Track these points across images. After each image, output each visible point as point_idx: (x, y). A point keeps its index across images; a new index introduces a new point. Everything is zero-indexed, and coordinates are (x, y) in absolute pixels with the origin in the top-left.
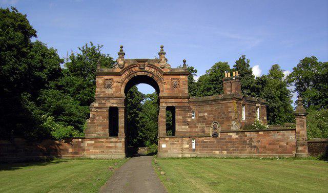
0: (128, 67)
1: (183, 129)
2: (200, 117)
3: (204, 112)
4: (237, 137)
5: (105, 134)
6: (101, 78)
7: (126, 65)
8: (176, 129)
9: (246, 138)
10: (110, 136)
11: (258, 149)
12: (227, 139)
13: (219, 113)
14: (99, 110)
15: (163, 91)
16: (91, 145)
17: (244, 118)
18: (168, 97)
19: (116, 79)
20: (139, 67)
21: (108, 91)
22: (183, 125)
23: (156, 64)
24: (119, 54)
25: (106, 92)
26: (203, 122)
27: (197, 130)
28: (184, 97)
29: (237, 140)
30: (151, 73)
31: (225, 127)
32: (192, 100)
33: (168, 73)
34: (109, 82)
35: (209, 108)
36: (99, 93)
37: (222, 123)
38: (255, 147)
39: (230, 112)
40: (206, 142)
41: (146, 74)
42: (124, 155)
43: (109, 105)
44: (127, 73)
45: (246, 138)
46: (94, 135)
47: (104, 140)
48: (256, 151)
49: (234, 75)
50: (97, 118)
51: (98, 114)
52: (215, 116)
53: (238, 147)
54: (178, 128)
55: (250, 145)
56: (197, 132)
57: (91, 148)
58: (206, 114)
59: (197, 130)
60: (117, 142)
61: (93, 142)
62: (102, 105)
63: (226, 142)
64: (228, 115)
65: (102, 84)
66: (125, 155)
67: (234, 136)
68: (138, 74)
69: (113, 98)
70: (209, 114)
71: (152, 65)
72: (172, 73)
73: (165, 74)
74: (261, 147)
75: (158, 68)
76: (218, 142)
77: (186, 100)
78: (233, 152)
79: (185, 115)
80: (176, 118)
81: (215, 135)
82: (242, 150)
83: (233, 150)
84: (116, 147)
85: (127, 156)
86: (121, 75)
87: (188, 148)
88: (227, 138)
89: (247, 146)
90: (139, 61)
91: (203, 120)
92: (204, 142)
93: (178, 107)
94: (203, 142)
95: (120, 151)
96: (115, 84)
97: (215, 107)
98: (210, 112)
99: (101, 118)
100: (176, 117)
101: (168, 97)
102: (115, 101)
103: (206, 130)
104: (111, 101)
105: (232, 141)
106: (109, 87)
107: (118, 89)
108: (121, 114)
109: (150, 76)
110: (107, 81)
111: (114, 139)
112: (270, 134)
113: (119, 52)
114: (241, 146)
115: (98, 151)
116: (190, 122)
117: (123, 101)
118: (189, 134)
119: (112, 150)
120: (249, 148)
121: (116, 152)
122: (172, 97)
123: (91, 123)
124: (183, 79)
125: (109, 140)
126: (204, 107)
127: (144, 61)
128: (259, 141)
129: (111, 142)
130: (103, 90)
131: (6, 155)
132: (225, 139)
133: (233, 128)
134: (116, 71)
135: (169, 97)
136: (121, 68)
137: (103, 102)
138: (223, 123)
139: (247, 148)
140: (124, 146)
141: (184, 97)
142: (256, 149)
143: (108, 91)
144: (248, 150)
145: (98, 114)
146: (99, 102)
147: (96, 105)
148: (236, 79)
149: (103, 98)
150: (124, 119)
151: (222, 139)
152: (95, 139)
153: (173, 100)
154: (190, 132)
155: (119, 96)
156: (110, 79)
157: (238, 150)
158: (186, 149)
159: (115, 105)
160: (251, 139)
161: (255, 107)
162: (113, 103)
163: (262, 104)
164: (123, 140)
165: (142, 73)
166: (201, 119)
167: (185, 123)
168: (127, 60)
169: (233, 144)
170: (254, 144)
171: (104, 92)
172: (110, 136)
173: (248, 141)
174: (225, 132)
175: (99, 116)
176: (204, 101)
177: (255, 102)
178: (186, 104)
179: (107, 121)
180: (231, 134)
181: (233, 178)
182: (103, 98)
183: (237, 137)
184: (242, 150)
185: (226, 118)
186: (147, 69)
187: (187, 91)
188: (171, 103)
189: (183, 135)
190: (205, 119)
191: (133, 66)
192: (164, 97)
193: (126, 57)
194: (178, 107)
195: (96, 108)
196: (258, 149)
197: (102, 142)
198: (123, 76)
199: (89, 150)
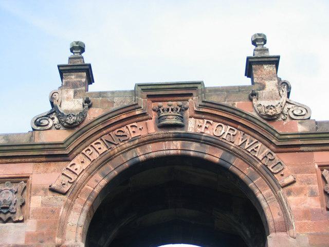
20: (160, 118)
24: (64, 71)
30: (214, 143)
41: (193, 149)
44: (99, 149)
73: (289, 145)
86: (66, 158)
96: (36, 202)
109: (216, 156)
156: (15, 180)
165: (174, 147)
186: (192, 126)
198: (79, 164)
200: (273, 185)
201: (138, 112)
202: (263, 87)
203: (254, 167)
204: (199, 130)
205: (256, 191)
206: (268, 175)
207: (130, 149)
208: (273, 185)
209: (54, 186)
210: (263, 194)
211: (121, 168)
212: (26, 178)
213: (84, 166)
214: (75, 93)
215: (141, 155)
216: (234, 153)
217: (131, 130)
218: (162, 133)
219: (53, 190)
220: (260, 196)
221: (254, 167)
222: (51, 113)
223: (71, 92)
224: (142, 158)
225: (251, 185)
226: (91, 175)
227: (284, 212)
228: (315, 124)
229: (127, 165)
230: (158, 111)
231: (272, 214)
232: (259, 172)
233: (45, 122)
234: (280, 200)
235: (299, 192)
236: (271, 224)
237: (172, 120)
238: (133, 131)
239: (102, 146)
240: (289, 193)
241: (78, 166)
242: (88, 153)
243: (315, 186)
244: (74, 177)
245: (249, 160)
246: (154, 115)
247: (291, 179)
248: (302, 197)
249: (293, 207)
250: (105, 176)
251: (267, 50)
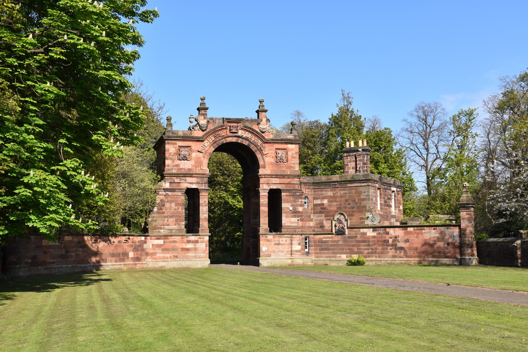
0: (214, 129)
1: (292, 223)
2: (315, 205)
3: (324, 198)
4: (374, 234)
5: (180, 230)
6: (172, 144)
7: (211, 127)
8: (283, 223)
9: (387, 237)
10: (188, 232)
11: (405, 252)
12: (359, 238)
13: (346, 200)
14: (170, 193)
15: (264, 167)
16: (159, 246)
17: (71, 152)
18: (271, 176)
19: (195, 146)
20: (230, 130)
21: (184, 164)
22: (292, 217)
23: (255, 127)
24: (198, 109)
25: (181, 167)
26: (321, 212)
27: (312, 224)
28: (294, 176)
29: (373, 239)
30: (246, 139)
31: (354, 220)
32: (305, 181)
33: (272, 140)
34: (184, 152)
35: (330, 193)
36: (170, 168)
37: (351, 215)
38: (402, 248)
39: (364, 200)
40: (325, 242)
41: (240, 141)
42: (209, 261)
43: (185, 185)
44: (212, 138)
45: (387, 237)
46: (162, 231)
47: (177, 238)
48: (402, 254)
49: (360, 144)
50: (167, 205)
51: (170, 199)
52: (340, 205)
53: (376, 249)
54: (287, 221)
55: (394, 246)
56: (311, 227)
57: (159, 251)
58: (325, 202)
59: (312, 224)
60: (197, 242)
61: (161, 242)
62: (174, 186)
63: (358, 241)
64: (360, 203)
65: (174, 154)
66: (210, 262)
67: (370, 233)
68: (229, 140)
69: (191, 175)
70: (331, 202)
71: (249, 128)
72: (277, 140)
73: (267, 142)
74: (410, 248)
75: (257, 132)
76: (345, 241)
77: (296, 181)
78: (369, 257)
79: (295, 201)
80: (283, 206)
81: (340, 232)
82: (382, 253)
83: (368, 253)
84: (196, 249)
85: (212, 263)
86: (202, 141)
87: (300, 251)
88: (359, 236)
89: (389, 248)
90: (230, 121)
91: (321, 209)
92: (323, 242)
93: (286, 191)
94: (321, 241)
95: (202, 255)
96: (194, 155)
97: (340, 192)
98: (332, 199)
99: (173, 205)
100: (283, 204)
101: (271, 176)
102: (194, 180)
103: (327, 224)
104: (189, 179)
105: (366, 240)
106: (185, 158)
107: (199, 163)
108: (204, 200)
109: (246, 143)
110: (182, 149)
111: (192, 238)
112: (423, 231)
113: (207, 111)
114: (380, 248)
115: (168, 255)
116: (302, 212)
117: (206, 180)
118: (300, 230)
119: (191, 254)
120: (393, 251)
121: (195, 257)
122: (277, 176)
123: (158, 213)
124: (292, 149)
125: (185, 239)
126: (323, 191)
127: (238, 121)
128: (407, 241)
129: (189, 242)
130: (177, 162)
131: (53, 263)
132: (356, 237)
133: (368, 222)
134: (196, 135)
135: (273, 175)
136: (203, 131)
137: (177, 180)
138: (352, 215)
139: (389, 250)
140: (208, 248)
141: (294, 176)
142: (402, 251)
143: (184, 164)
144: (392, 252)
145: (170, 199)
146: (170, 181)
147: (167, 185)
148: (363, 150)
149: (177, 175)
150: (207, 208)
151: (351, 237)
152: (166, 237)
153: (277, 180)
154: (302, 227)
155: (201, 172)
156: (188, 147)
157: (375, 253)
158: (297, 251)
159: (194, 186)
160: (396, 237)
161: (390, 192)
162: (191, 183)
163: (398, 187)
164: (207, 238)
165: (234, 140)
166: (318, 209)
167: (295, 213)
168: (212, 119)
169: (369, 245)
170: (400, 245)
171: (177, 165)
172: (188, 232)
173: (391, 241)
174: (356, 228)
175: (171, 202)
176: (322, 183)
177: (390, 185)
178: (297, 187)
179: (182, 211)
180: (365, 230)
181: (403, 300)
182: (177, 175)
183: (374, 234)
184: (383, 253)
185: (358, 207)
186: (240, 133)
187: (297, 168)
188: (275, 184)
189: (293, 232)
190: (325, 208)
191: (222, 128)
192: (266, 176)
193: (210, 114)
194: (286, 191)
195: (165, 190)
196: (405, 252)
197: (175, 242)
198: (206, 143)
199: (154, 254)
200: (263, 155)
201: (224, 127)
202: (262, 121)
203: (257, 148)
204: (242, 134)
205: (257, 155)
206: (261, 150)
207: (221, 139)
208: (263, 155)
209: (199, 150)
210: (259, 156)
211: (219, 145)
212: (190, 147)
213: (208, 144)
214: (204, 117)
215: (224, 141)
216: (252, 143)
217: (222, 133)
218: (231, 134)
219: (199, 152)
220: (258, 157)
221: (257, 148)
222: (197, 124)
223: (203, 117)
224: (225, 142)
225: (256, 153)
226: (210, 147)
227: (264, 163)
228: (221, 121)
229: (220, 144)
230: (230, 127)
231: (261, 163)
232: (258, 149)
233: (195, 128)
234: (263, 159)
235: (269, 156)
236: (260, 166)
237: (234, 131)
238: (223, 133)
239: (213, 137)
240: (266, 157)
241: (206, 144)
242: (209, 140)
243: (273, 155)
244: (205, 147)
245: (256, 146)
246: (228, 128)
247: (267, 153)
248: (270, 158)
249: (267, 161)
250: (214, 147)
251: (264, 106)
